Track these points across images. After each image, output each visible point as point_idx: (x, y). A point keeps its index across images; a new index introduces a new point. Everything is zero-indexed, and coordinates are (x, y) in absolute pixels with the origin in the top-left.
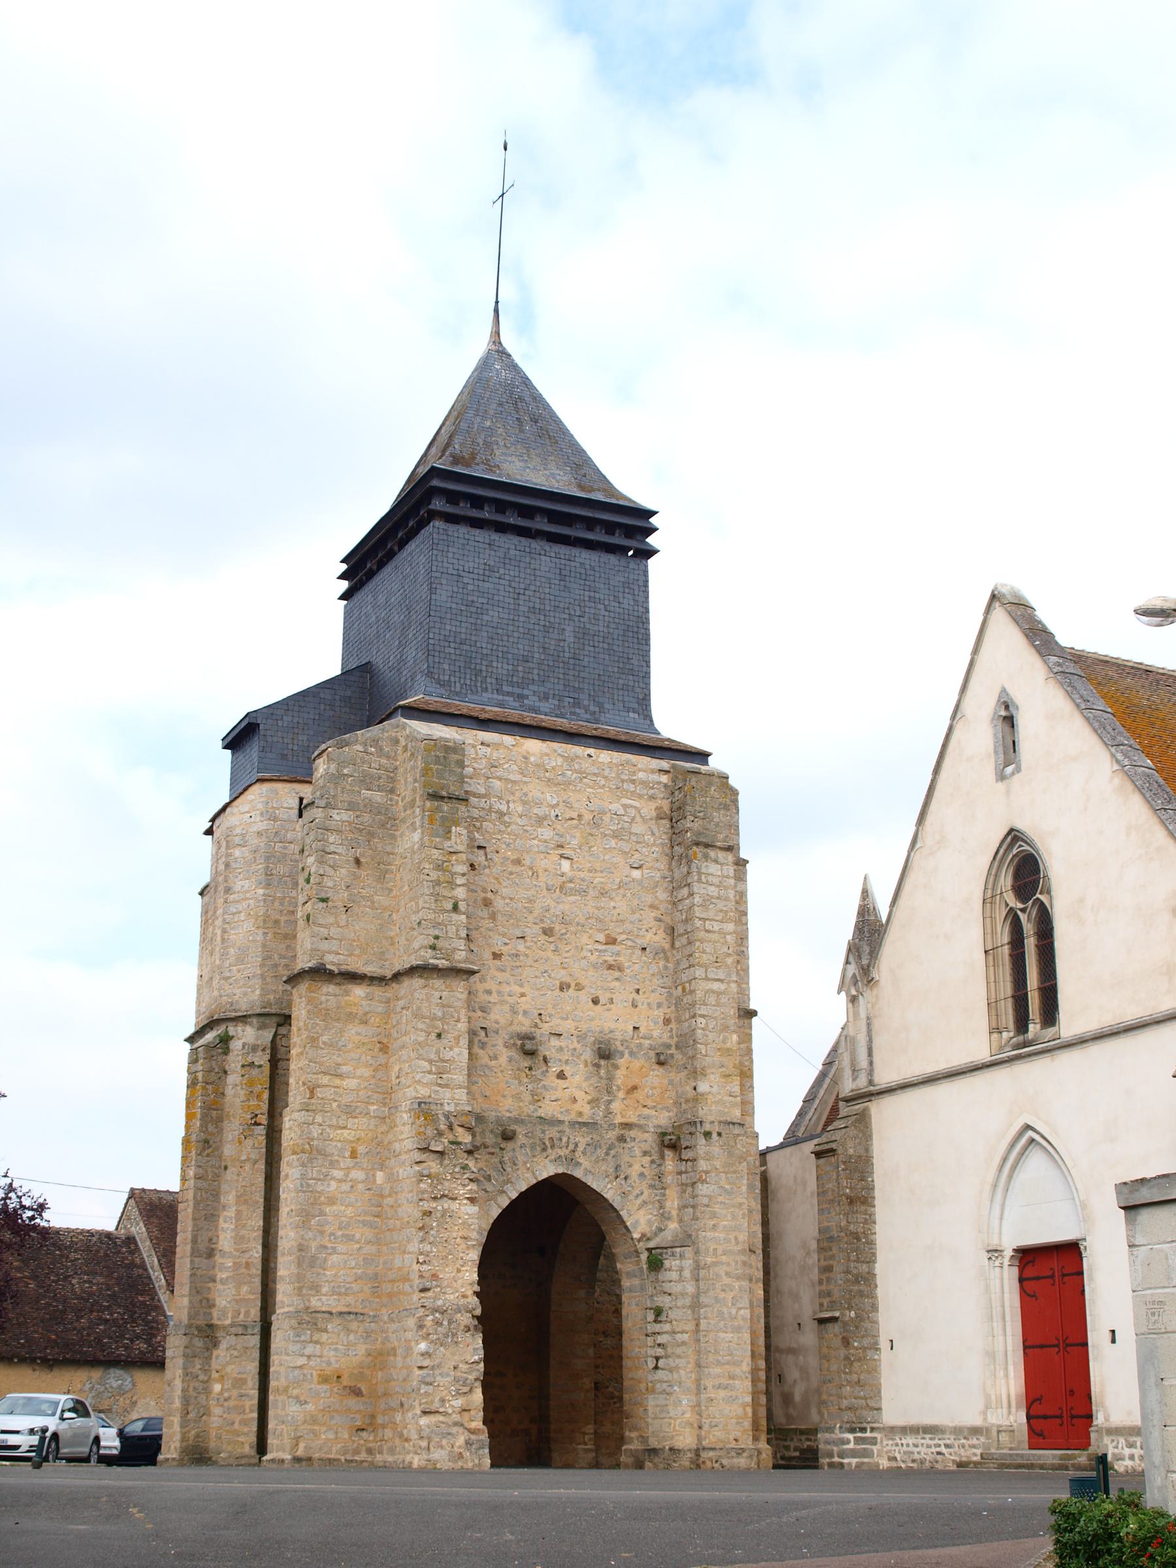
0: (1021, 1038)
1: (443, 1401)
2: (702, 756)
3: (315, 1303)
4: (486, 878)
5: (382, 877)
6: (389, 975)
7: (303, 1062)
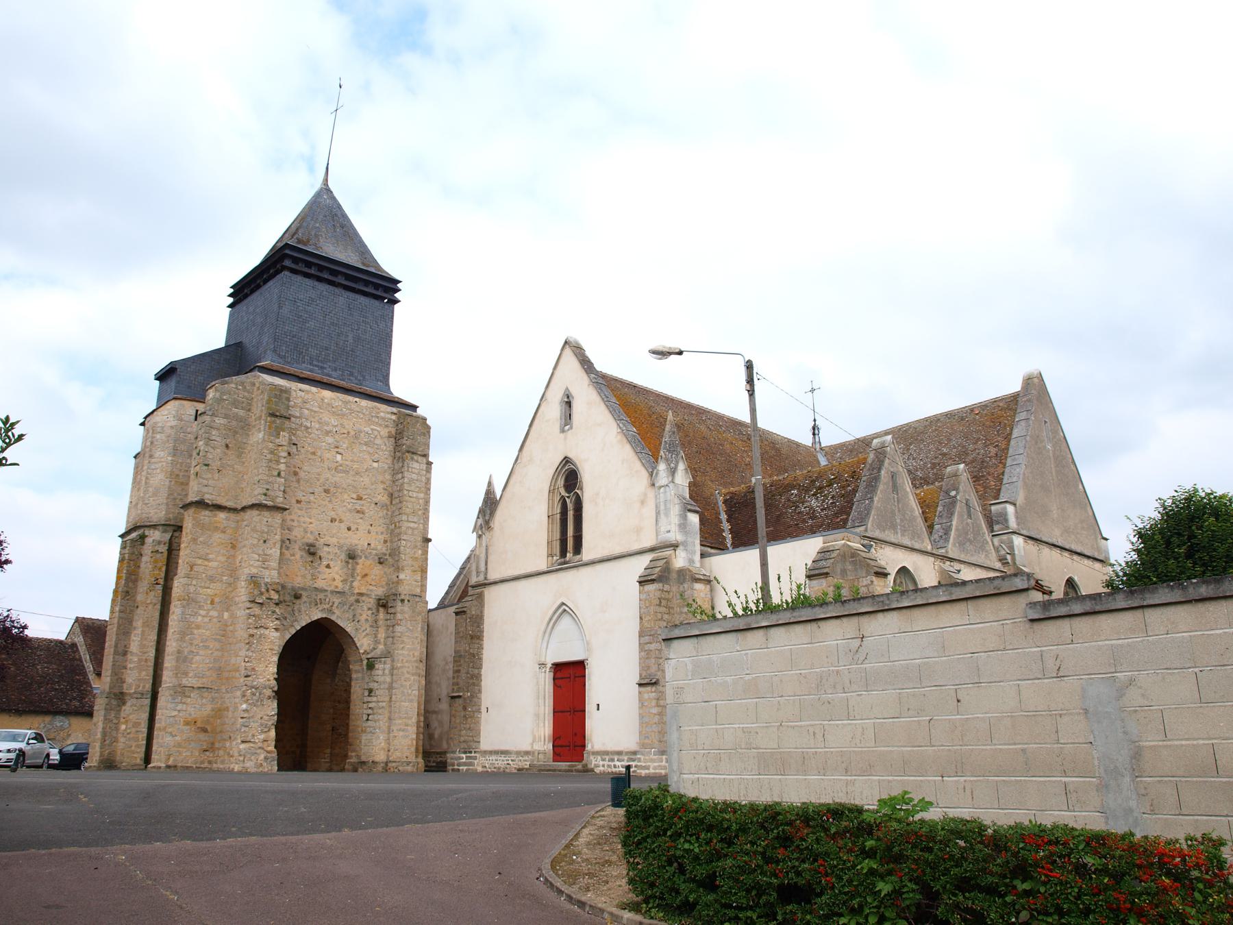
2: (414, 408)
3: (185, 682)
4: (296, 460)
5: (239, 456)
7: (188, 551)
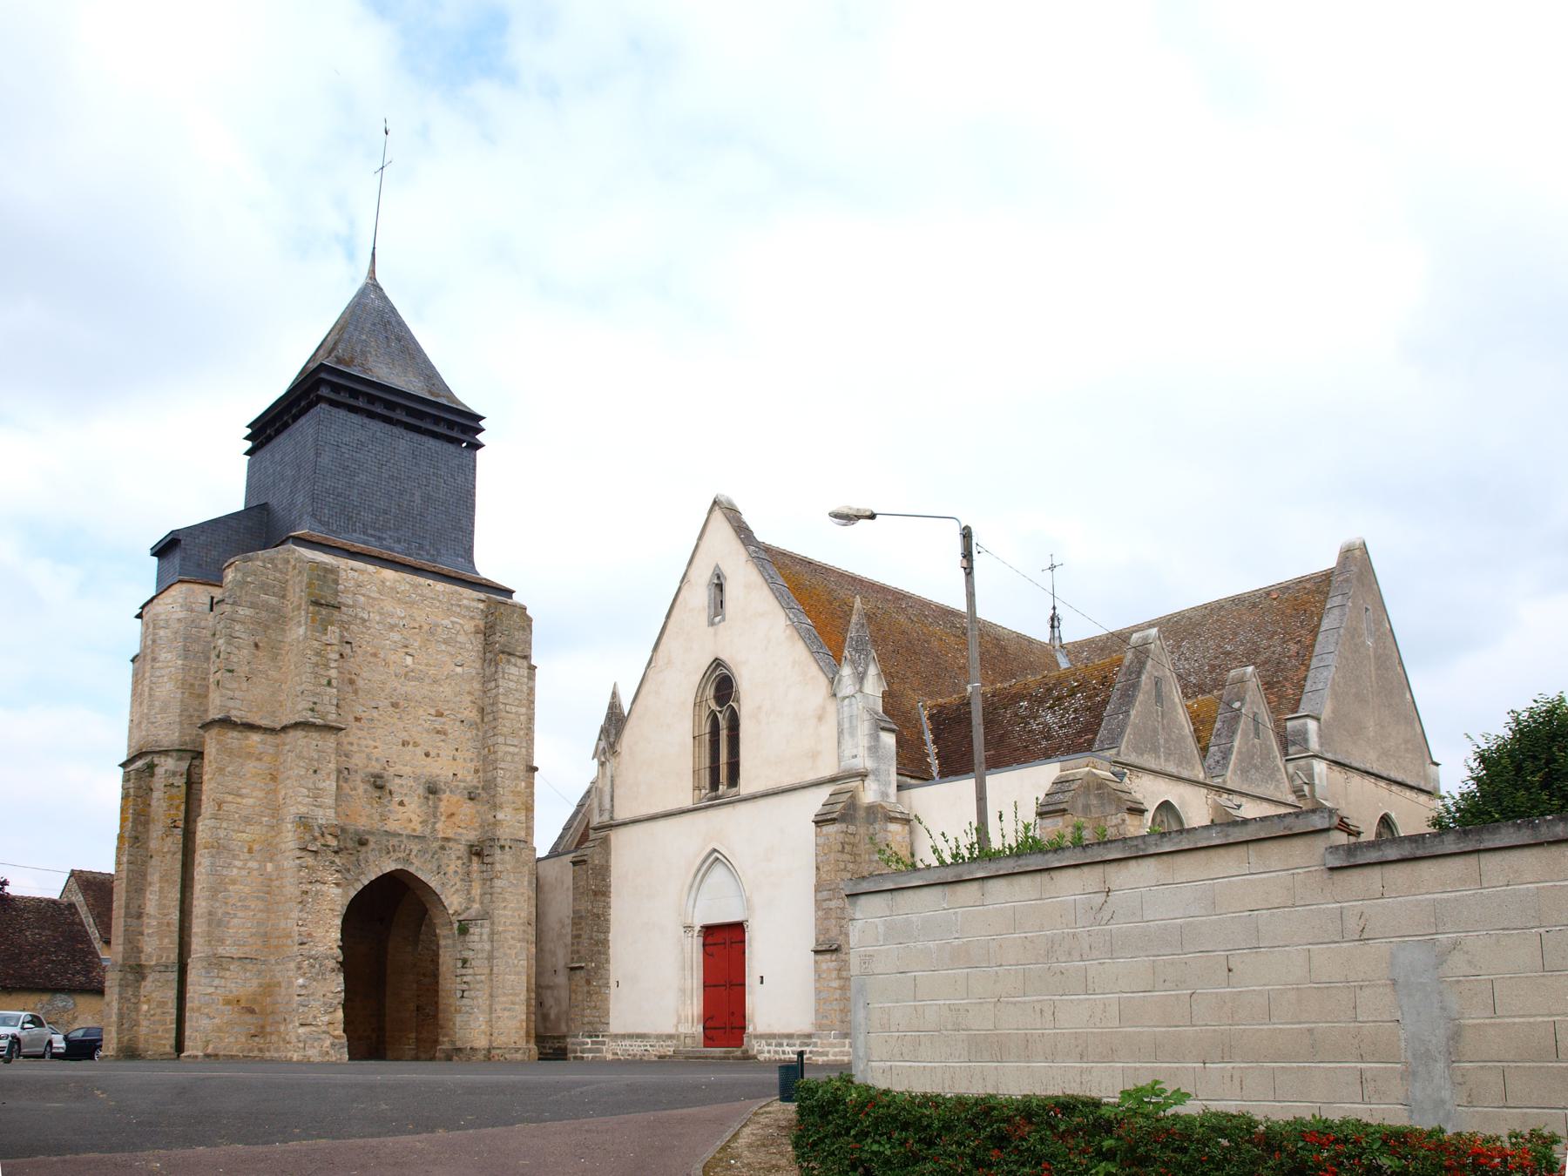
2: (509, 593)
3: (221, 951)
5: (274, 658)
7: (213, 785)
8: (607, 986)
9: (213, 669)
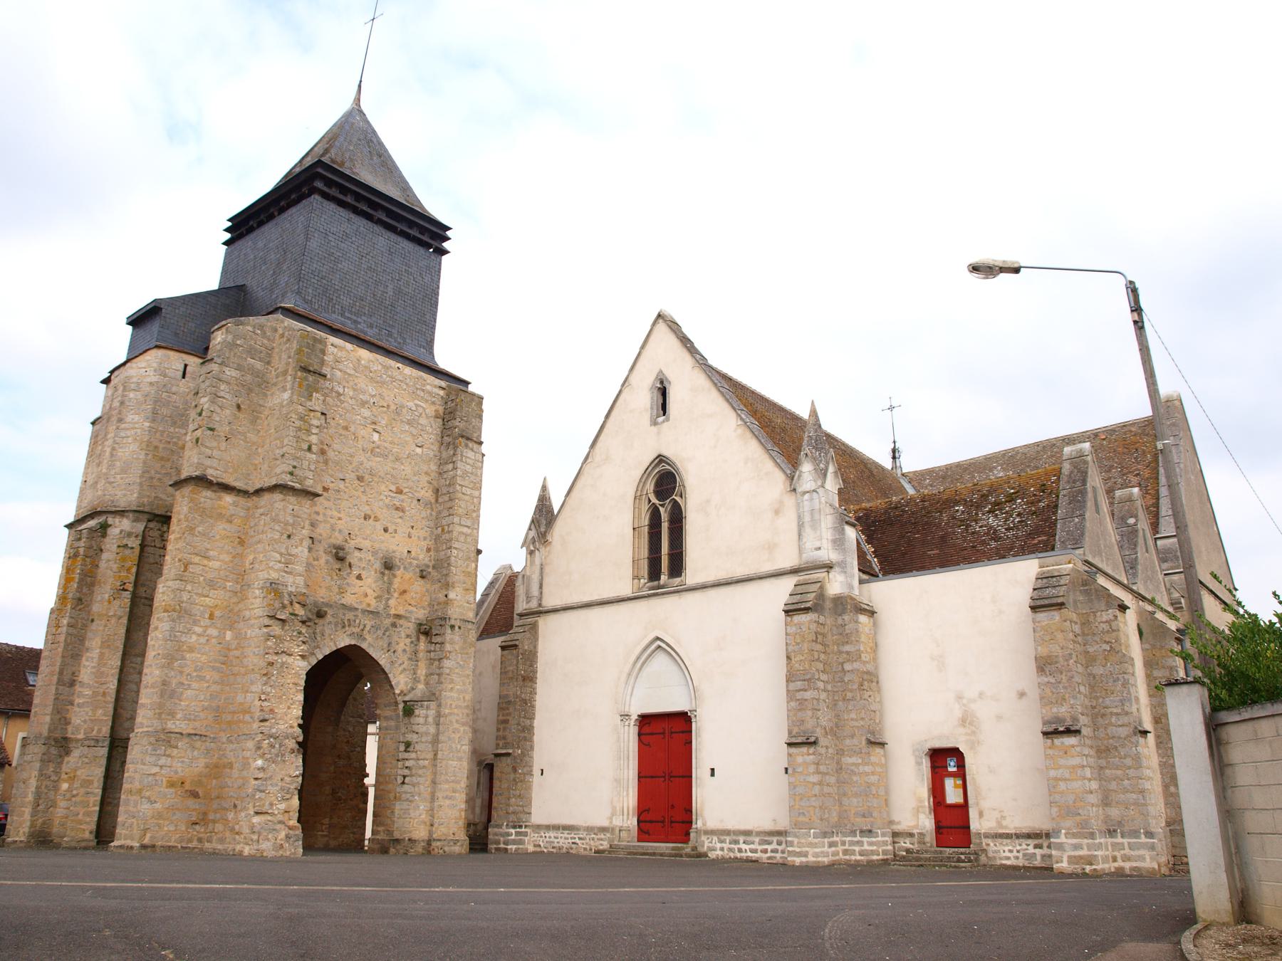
0: (656, 583)
1: (271, 805)
2: (466, 383)
3: (170, 725)
5: (254, 421)
6: (251, 490)
7: (181, 544)
8: (530, 773)
9: (191, 427)
